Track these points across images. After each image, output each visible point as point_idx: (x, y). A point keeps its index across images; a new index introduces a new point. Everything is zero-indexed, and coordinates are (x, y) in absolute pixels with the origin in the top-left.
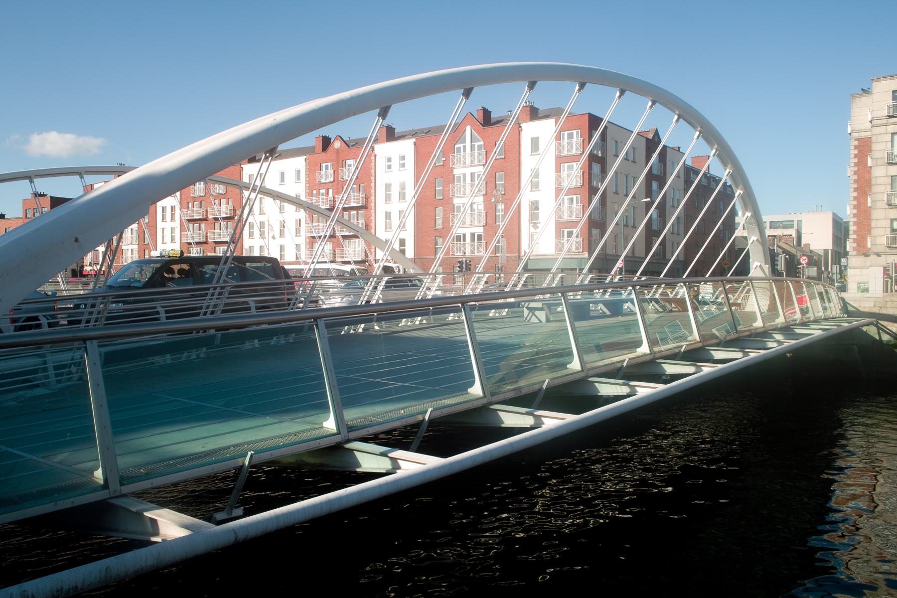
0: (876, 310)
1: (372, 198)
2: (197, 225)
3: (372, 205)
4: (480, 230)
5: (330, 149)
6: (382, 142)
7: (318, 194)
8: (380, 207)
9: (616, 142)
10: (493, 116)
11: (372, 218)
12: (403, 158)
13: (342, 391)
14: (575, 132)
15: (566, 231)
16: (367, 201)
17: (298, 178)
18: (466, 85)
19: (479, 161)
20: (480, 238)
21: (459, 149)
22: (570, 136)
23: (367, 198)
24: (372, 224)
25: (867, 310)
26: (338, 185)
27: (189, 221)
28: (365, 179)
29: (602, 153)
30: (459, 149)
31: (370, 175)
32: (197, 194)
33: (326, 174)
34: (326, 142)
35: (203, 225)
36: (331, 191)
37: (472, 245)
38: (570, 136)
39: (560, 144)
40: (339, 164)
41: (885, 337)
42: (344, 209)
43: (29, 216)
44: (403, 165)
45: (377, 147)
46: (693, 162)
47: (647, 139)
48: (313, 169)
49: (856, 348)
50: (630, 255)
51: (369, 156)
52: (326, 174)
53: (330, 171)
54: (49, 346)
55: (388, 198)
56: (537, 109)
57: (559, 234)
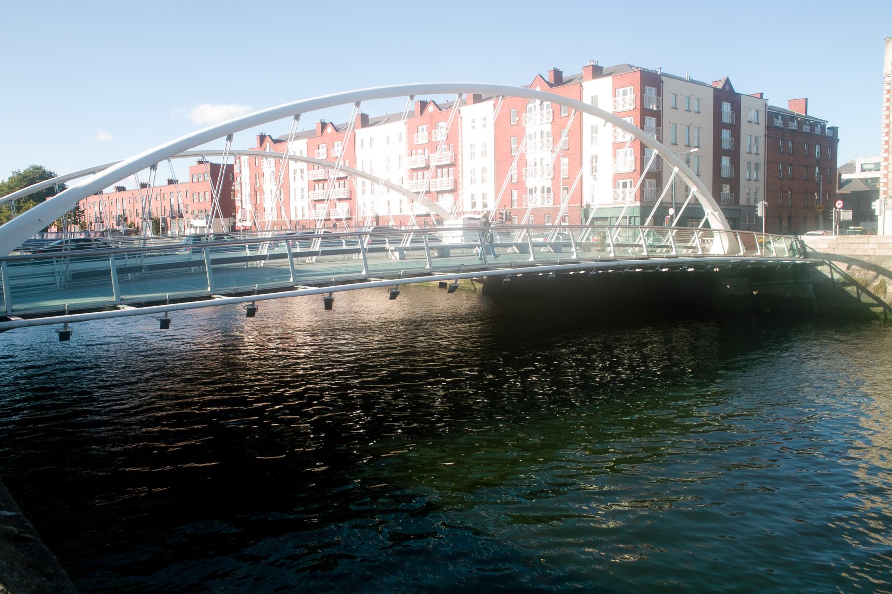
0: (830, 252)
1: (460, 156)
2: (321, 184)
3: (460, 162)
4: (548, 184)
5: (425, 113)
6: (588, 80)
7: (416, 154)
8: (467, 165)
9: (676, 95)
10: (564, 75)
11: (460, 174)
12: (485, 119)
13: (120, 283)
14: (628, 88)
15: (621, 182)
16: (456, 159)
17: (400, 139)
18: (357, 99)
19: (548, 119)
20: (548, 190)
21: (530, 109)
22: (625, 93)
23: (455, 157)
24: (460, 180)
25: (822, 251)
26: (432, 146)
27: (315, 181)
28: (453, 139)
29: (657, 107)
30: (530, 109)
31: (458, 135)
32: (420, 142)
33: (422, 137)
34: (423, 105)
35: (326, 184)
36: (426, 151)
37: (542, 197)
38: (625, 93)
39: (615, 101)
40: (433, 126)
41: (836, 276)
42: (437, 167)
43: (195, 180)
44: (485, 125)
45: (463, 109)
46: (790, 106)
47: (715, 89)
48: (412, 130)
49: (811, 286)
50: (693, 202)
51: (456, 118)
52: (422, 137)
53: (426, 133)
54: (273, 301)
55: (472, 155)
56: (601, 68)
57: (615, 185)
